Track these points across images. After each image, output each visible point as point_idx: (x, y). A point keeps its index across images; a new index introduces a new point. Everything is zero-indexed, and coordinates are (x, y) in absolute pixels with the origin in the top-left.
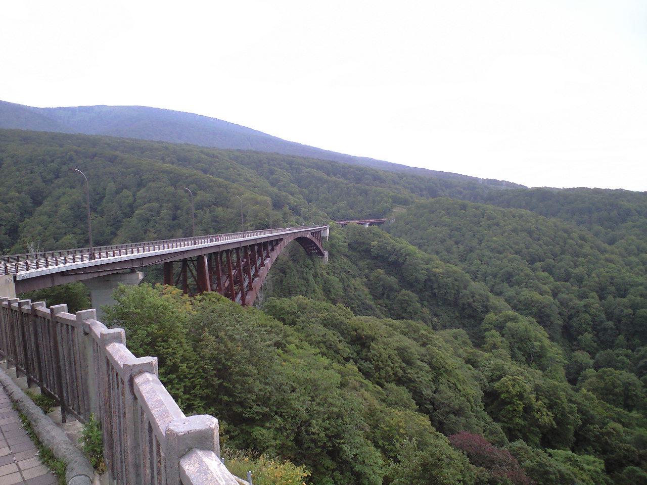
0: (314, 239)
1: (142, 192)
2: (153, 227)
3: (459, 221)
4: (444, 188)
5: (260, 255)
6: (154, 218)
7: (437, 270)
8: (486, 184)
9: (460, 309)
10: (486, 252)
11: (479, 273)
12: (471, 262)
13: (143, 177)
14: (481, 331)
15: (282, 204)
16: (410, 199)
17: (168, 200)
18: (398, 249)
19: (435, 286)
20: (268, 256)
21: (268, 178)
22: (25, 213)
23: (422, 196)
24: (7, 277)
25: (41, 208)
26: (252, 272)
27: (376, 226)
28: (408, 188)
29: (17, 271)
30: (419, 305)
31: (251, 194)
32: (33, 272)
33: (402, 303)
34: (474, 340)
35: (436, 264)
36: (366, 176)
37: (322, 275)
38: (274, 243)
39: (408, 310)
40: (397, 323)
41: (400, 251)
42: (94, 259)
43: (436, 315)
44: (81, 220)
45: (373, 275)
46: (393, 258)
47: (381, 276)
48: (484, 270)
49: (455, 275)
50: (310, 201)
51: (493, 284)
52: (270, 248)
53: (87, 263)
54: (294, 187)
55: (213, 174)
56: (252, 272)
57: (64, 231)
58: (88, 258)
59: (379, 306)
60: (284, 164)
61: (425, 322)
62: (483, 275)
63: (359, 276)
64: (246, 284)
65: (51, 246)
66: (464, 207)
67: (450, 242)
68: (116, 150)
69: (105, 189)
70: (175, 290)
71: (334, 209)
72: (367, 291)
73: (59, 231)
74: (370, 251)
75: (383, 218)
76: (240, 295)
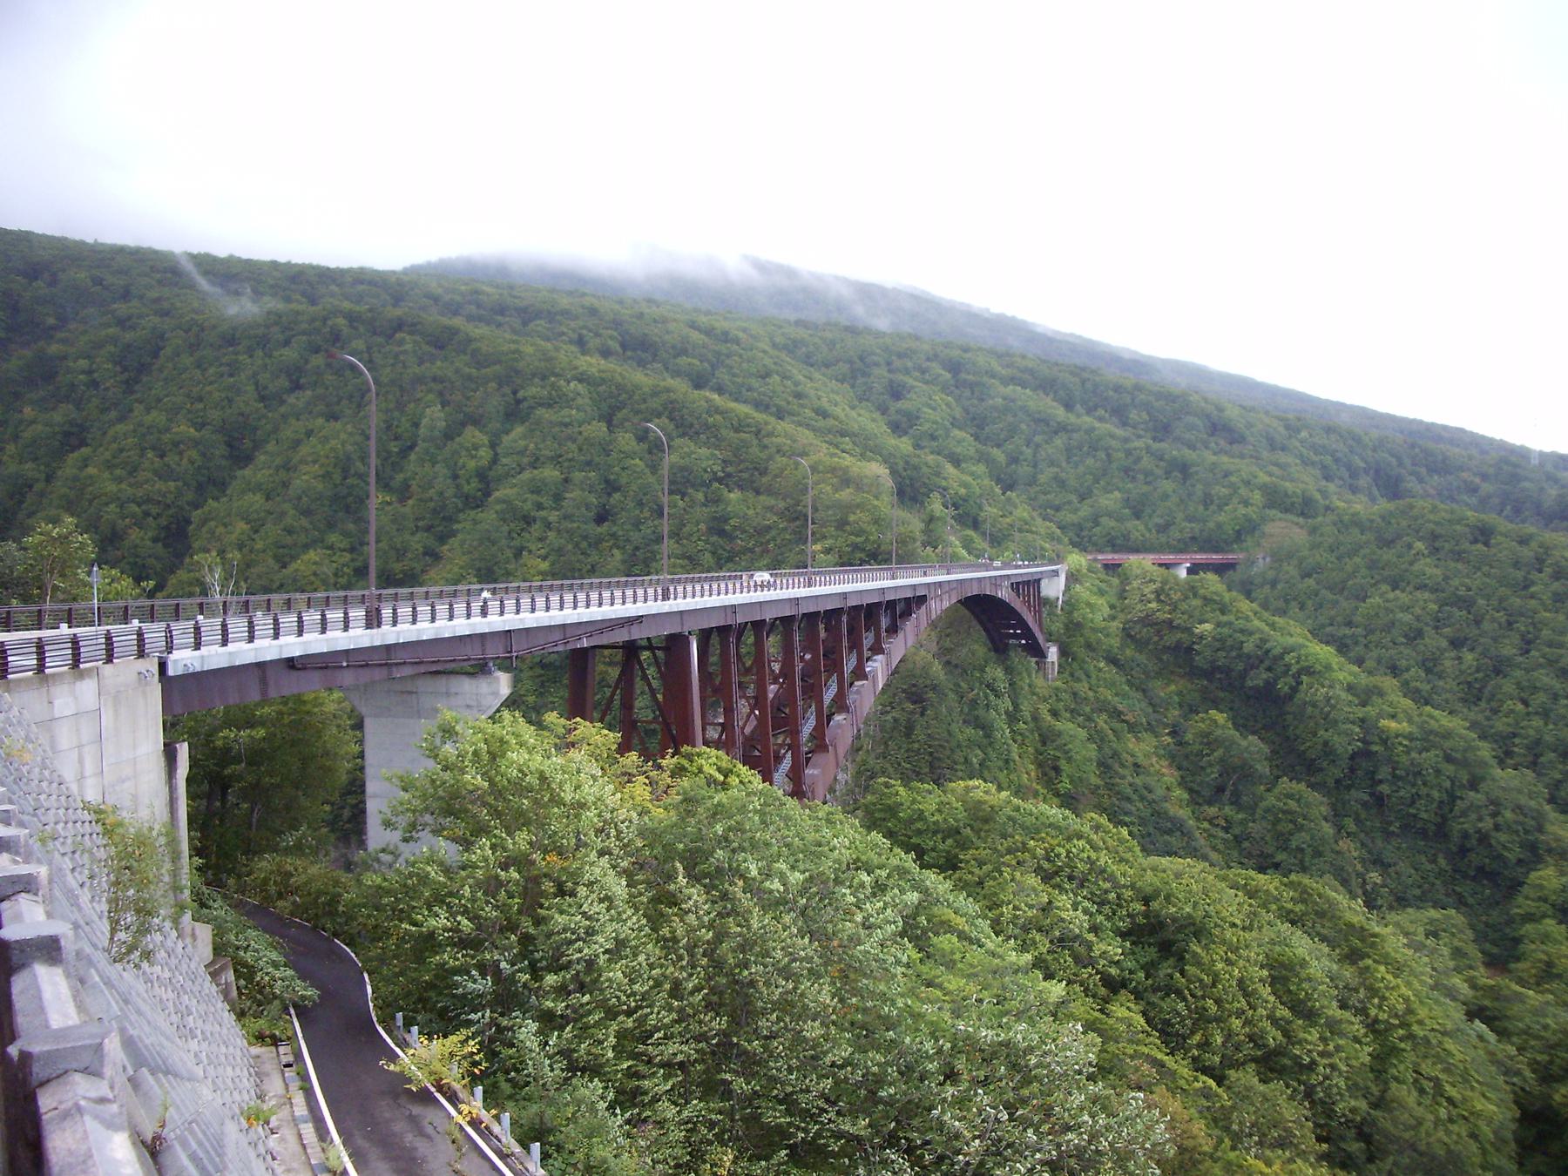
0: (1017, 604)
1: (516, 436)
2: (540, 540)
3: (1468, 576)
4: (1423, 471)
5: (855, 645)
6: (543, 513)
7: (1393, 725)
8: (1549, 467)
9: (1454, 849)
10: (1546, 680)
11: (1517, 741)
12: (1494, 704)
13: (521, 394)
14: (1510, 922)
15: (923, 490)
16: (1318, 496)
17: (589, 463)
18: (1277, 651)
19: (1384, 772)
20: (877, 649)
21: (884, 410)
22: (211, 484)
23: (1354, 490)
24: (142, 665)
25: (247, 472)
26: (829, 695)
27: (1211, 577)
28: (1313, 464)
29: (170, 648)
30: (1328, 829)
31: (833, 455)
32: (214, 656)
33: (1279, 820)
34: (1488, 946)
35: (1391, 705)
36: (1190, 419)
37: (1035, 718)
38: (901, 609)
39: (1294, 844)
40: (1267, 882)
41: (1281, 657)
42: (379, 626)
43: (1379, 862)
44: (347, 509)
45: (1196, 726)
46: (1258, 678)
47: (1219, 732)
48: (1531, 732)
49: (1447, 744)
50: (1008, 486)
51: (1559, 777)
52: (884, 622)
53: (359, 637)
54: (963, 441)
55: (720, 390)
56: (829, 695)
57: (302, 539)
58: (363, 623)
59: (1206, 825)
60: (937, 369)
61: (1345, 882)
62: (1528, 748)
63: (1150, 728)
64: (807, 728)
65: (267, 584)
66: (1484, 534)
67: (1434, 641)
68: (455, 313)
69: (416, 425)
70: (598, 735)
71: (1082, 514)
72: (1170, 776)
73: (289, 540)
74: (1190, 650)
75: (1232, 551)
76: (787, 764)
